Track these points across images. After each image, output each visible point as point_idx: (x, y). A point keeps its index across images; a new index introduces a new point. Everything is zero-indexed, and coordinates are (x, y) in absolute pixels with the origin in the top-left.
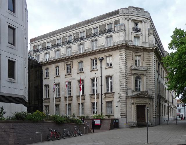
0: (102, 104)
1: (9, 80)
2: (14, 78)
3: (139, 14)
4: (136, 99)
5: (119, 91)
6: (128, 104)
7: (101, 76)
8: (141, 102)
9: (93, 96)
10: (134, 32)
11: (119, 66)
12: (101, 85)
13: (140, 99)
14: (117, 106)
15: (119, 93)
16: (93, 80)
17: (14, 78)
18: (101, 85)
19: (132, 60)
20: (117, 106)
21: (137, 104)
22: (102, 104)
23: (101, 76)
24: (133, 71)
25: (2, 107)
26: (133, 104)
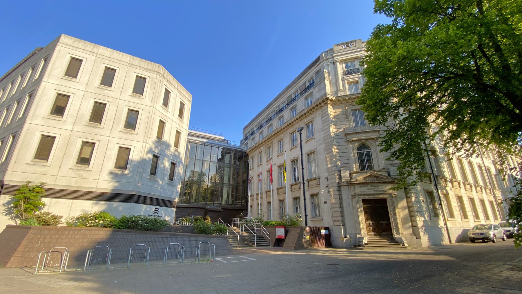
0: (305, 199)
1: (123, 131)
2: (167, 107)
3: (352, 49)
4: (358, 186)
5: (326, 175)
6: (344, 196)
7: (302, 154)
8: (372, 192)
9: (297, 186)
10: (345, 76)
11: (321, 133)
12: (303, 169)
13: (370, 186)
14: (325, 203)
15: (326, 178)
16: (280, 167)
17: (167, 107)
18: (303, 169)
19: (346, 120)
20: (325, 203)
21: (362, 197)
22: (305, 199)
23: (302, 154)
24: (348, 137)
25: (376, 12)
26: (353, 196)
